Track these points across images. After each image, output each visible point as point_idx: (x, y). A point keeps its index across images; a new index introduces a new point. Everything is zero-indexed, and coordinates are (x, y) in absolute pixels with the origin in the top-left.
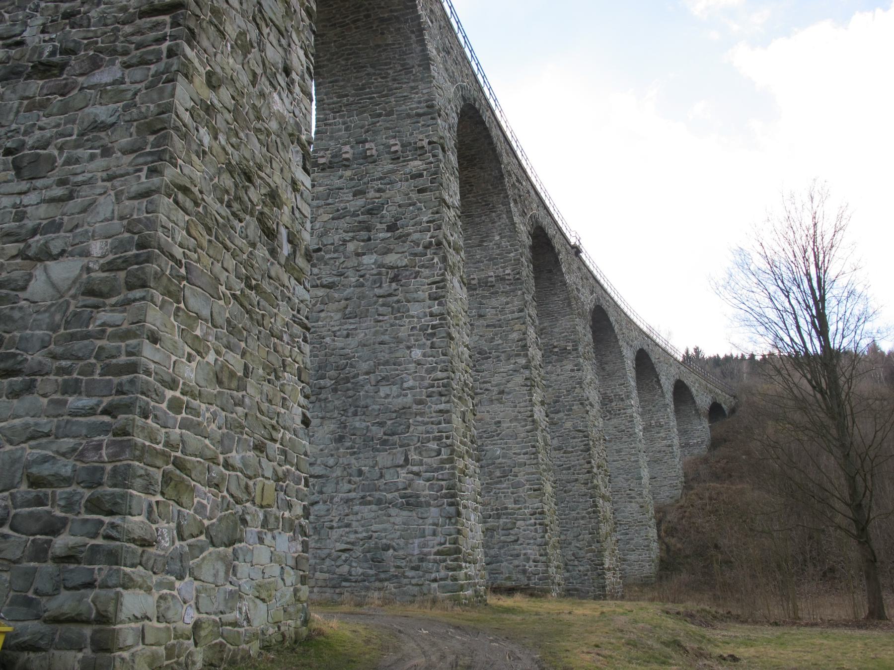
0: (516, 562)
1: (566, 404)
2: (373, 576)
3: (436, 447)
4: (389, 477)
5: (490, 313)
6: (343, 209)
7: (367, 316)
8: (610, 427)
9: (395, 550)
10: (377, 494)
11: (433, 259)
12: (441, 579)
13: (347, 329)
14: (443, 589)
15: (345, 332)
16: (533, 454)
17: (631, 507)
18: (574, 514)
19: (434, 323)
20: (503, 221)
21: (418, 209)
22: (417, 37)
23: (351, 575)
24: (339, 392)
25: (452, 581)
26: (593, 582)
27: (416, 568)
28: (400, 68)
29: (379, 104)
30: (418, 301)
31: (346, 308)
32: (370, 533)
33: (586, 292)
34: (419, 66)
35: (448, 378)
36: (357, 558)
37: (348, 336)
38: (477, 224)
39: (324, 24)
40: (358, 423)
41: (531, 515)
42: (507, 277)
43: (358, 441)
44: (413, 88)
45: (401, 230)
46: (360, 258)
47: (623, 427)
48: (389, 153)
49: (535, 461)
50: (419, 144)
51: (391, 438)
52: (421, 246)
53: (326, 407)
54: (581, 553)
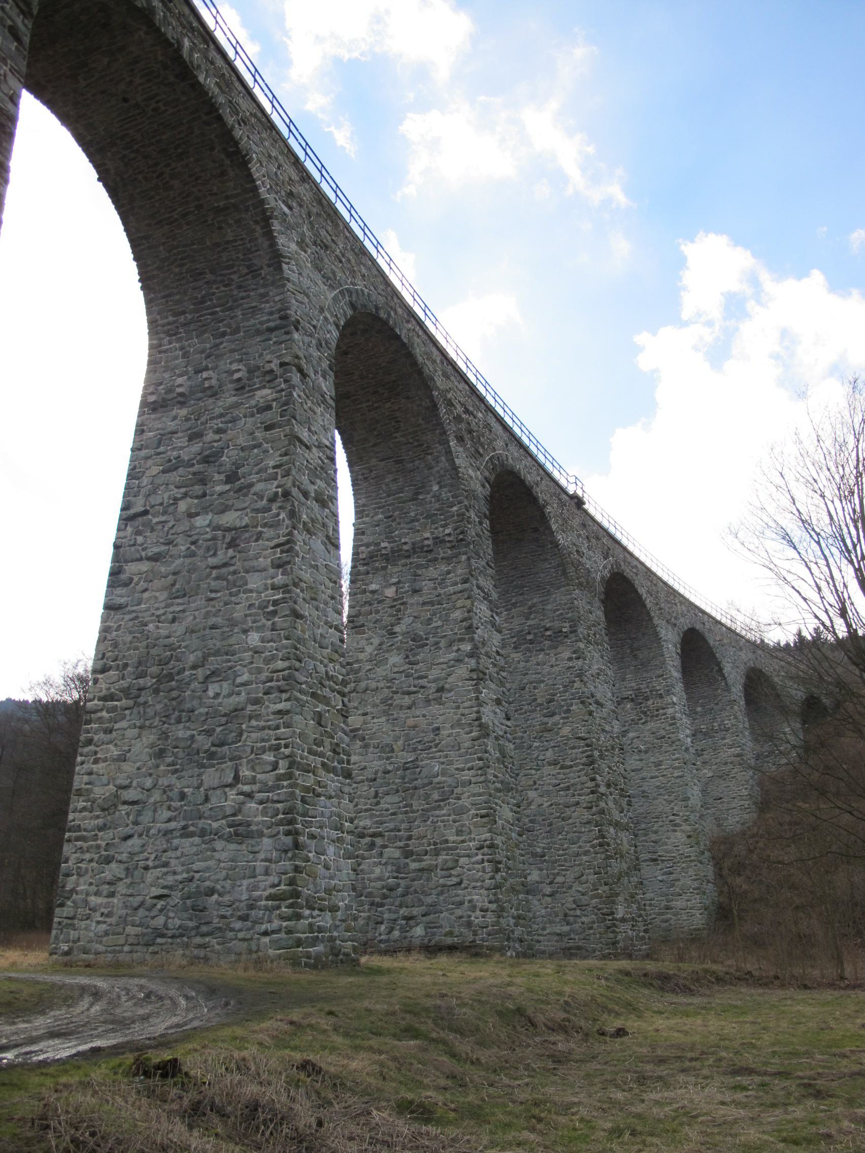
0: (459, 912)
1: (562, 703)
2: (193, 929)
3: (272, 759)
4: (215, 800)
5: (426, 585)
6: (176, 459)
7: (197, 594)
8: (647, 734)
9: (220, 895)
10: (201, 823)
11: (278, 515)
12: (273, 932)
13: (173, 612)
14: (276, 944)
15: (170, 616)
16: (480, 769)
17: (676, 838)
18: (574, 848)
19: (275, 597)
20: (441, 465)
21: (264, 452)
22: (263, 228)
23: (167, 929)
24: (162, 694)
25: (286, 933)
26: (600, 938)
27: (244, 918)
28: (246, 271)
29: (223, 320)
30: (258, 571)
31: (173, 585)
32: (192, 874)
33: (597, 557)
34: (269, 266)
35: (289, 668)
36: (175, 906)
37: (174, 620)
38: (410, 471)
39: (147, 222)
40: (181, 733)
41: (477, 849)
42: (447, 539)
43: (181, 755)
44: (263, 296)
45: (242, 480)
46: (192, 520)
47: (663, 733)
48: (232, 382)
49: (482, 779)
50: (268, 367)
51: (219, 749)
52: (265, 499)
53: (145, 713)
54: (584, 900)
